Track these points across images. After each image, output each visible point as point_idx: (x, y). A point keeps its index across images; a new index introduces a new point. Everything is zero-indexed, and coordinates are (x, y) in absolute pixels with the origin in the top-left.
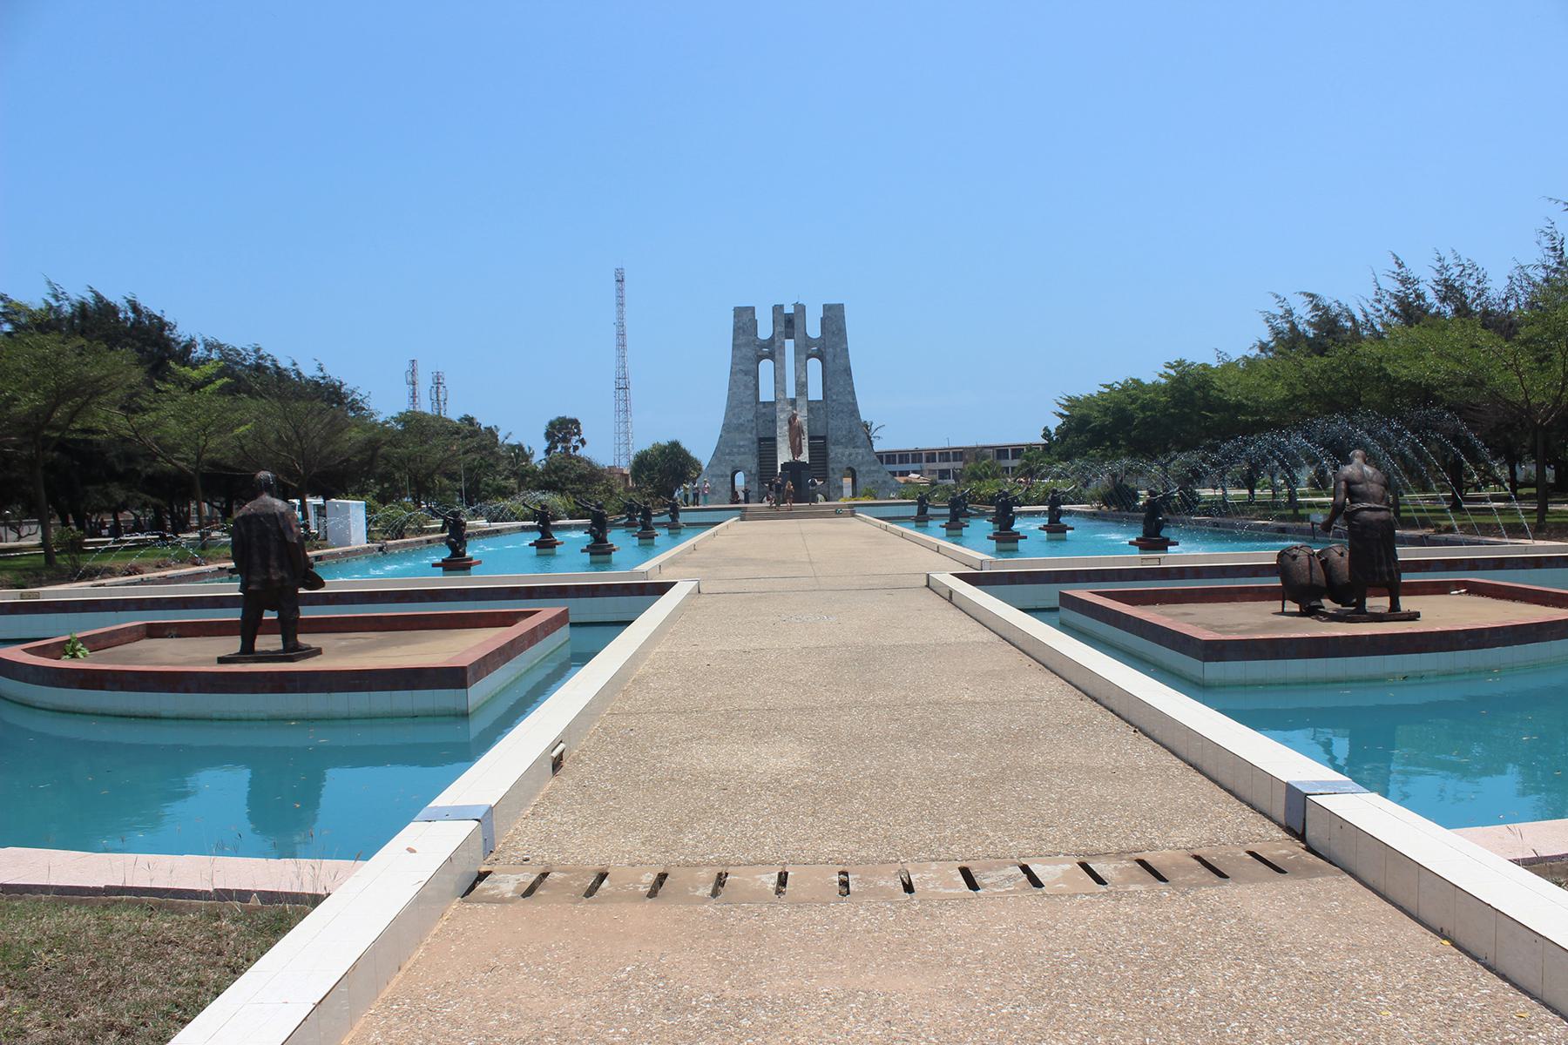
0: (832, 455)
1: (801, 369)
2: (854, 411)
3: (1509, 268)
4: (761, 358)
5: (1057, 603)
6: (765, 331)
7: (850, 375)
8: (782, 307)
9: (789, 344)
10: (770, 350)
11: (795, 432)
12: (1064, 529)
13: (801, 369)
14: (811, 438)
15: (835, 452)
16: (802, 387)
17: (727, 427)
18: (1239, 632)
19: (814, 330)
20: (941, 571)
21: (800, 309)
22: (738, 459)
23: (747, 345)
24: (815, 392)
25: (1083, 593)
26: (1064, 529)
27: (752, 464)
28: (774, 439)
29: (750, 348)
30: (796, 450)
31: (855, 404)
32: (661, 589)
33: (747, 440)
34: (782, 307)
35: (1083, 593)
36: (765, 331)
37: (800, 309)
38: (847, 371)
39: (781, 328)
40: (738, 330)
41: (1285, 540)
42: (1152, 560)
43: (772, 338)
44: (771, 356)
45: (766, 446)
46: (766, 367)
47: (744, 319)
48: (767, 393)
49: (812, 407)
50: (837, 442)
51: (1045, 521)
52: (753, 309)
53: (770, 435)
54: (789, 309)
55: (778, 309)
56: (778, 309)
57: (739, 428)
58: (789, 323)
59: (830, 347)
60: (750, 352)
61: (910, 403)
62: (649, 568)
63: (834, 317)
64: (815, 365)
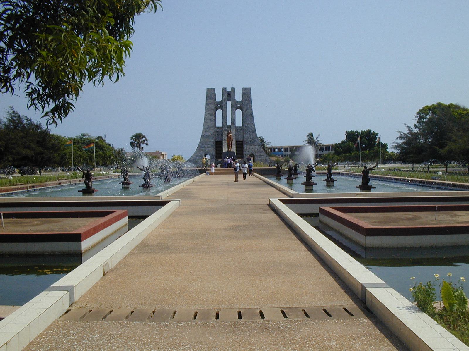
0: (245, 148)
1: (233, 113)
2: (254, 131)
3: (94, 188)
4: (217, 109)
5: (318, 212)
6: (219, 98)
7: (253, 116)
8: (226, 88)
9: (229, 104)
10: (221, 106)
11: (229, 140)
12: (333, 181)
13: (233, 113)
14: (237, 142)
15: (246, 147)
16: (233, 121)
17: (203, 136)
18: (446, 223)
19: (238, 98)
20: (274, 198)
21: (233, 90)
22: (207, 149)
23: (212, 104)
24: (239, 123)
25: (327, 208)
26: (333, 181)
27: (213, 152)
28: (222, 142)
29: (213, 105)
30: (229, 146)
31: (255, 128)
32: (163, 203)
33: (211, 141)
34: (226, 88)
35: (327, 208)
36: (219, 98)
37: (233, 90)
38: (252, 115)
39: (225, 97)
40: (208, 97)
41: (467, 183)
42: (366, 195)
43: (222, 101)
44: (221, 108)
45: (218, 145)
46: (219, 112)
47: (210, 94)
48: (219, 123)
49: (237, 129)
50: (247, 143)
51: (326, 177)
52: (214, 89)
53: (220, 140)
54: (229, 90)
55: (224, 89)
56: (224, 89)
57: (208, 137)
58: (229, 95)
59: (245, 104)
60: (212, 106)
61: (276, 127)
62: (163, 196)
63: (247, 93)
64: (239, 112)
